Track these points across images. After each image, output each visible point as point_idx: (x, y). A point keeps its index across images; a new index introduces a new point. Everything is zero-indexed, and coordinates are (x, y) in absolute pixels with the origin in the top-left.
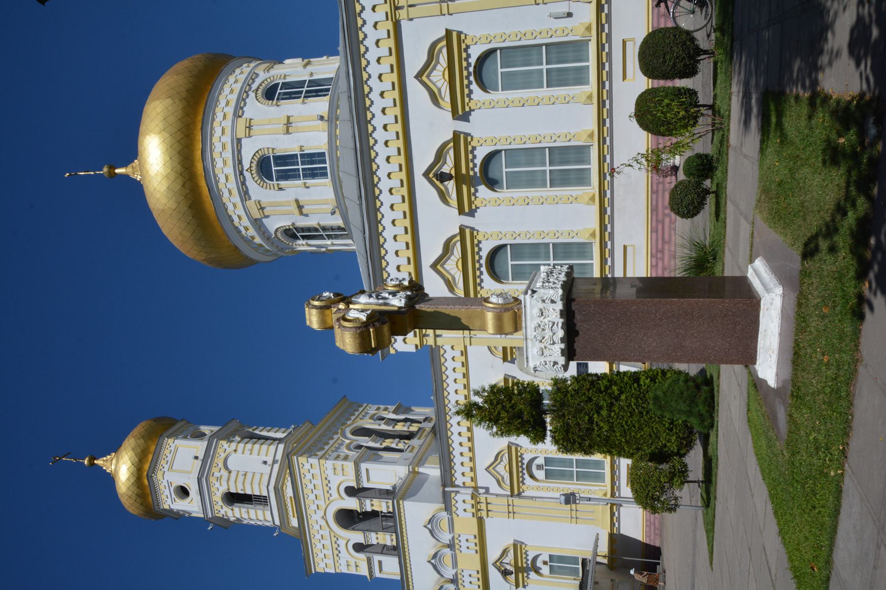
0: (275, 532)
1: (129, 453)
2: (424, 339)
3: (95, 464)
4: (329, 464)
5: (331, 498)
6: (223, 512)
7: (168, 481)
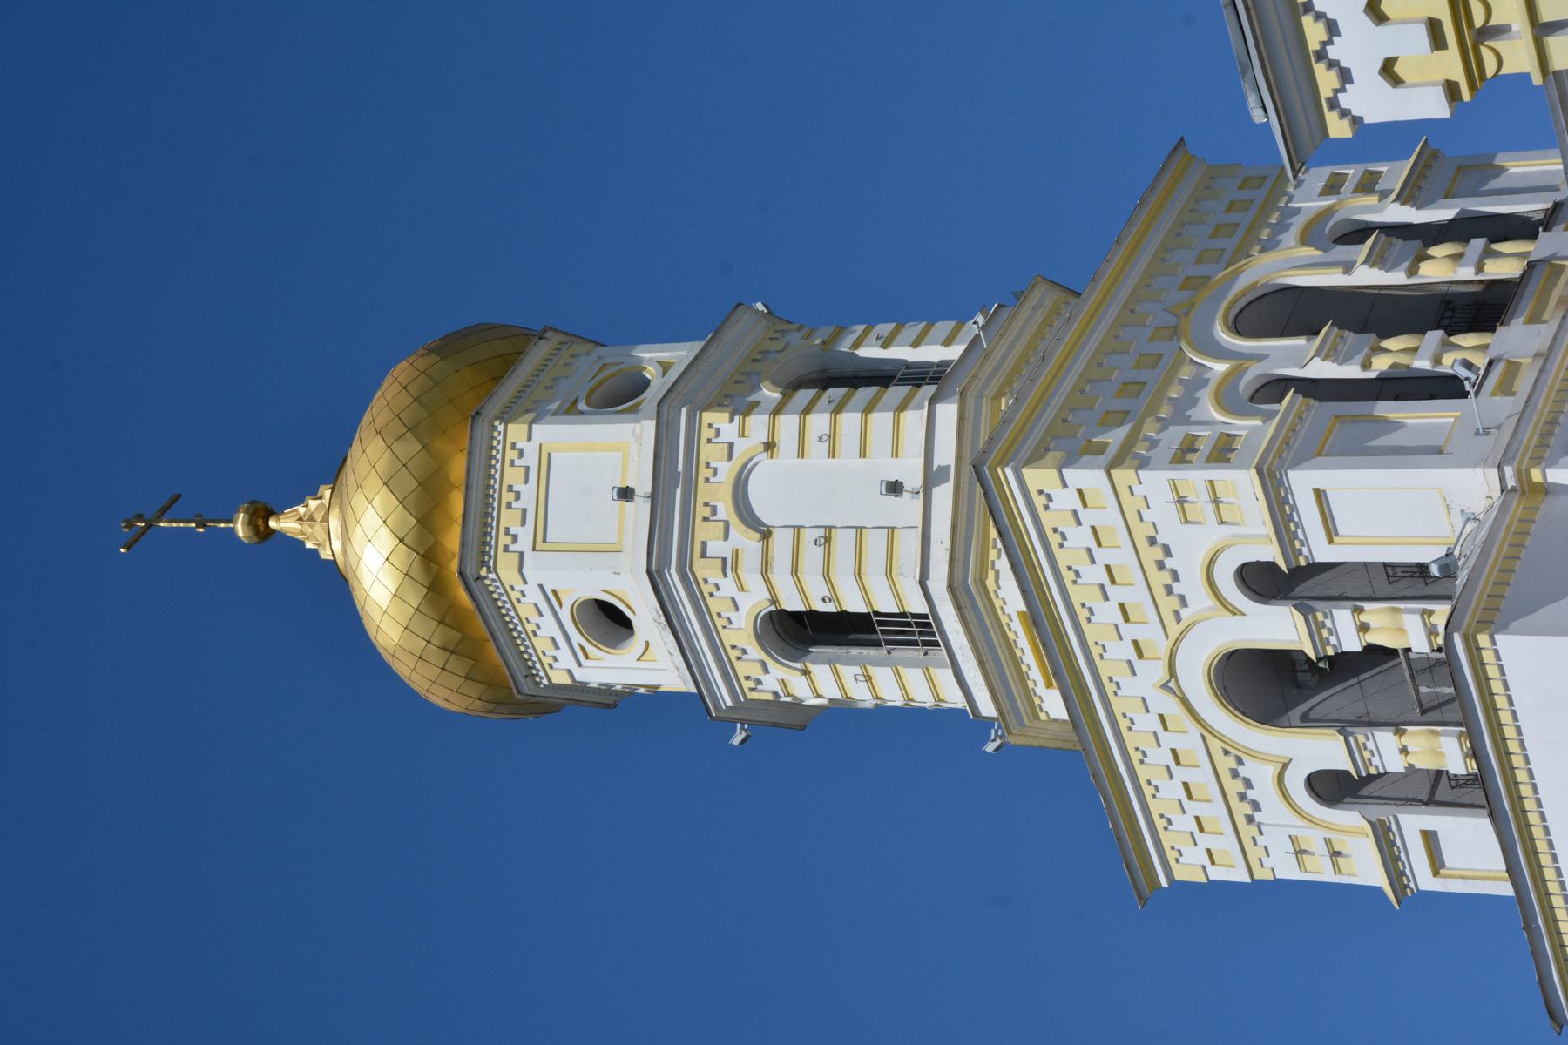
0: (986, 739)
1: (377, 501)
2: (1484, 50)
3: (273, 532)
4: (1155, 483)
5: (1184, 613)
6: (771, 683)
7: (541, 587)
